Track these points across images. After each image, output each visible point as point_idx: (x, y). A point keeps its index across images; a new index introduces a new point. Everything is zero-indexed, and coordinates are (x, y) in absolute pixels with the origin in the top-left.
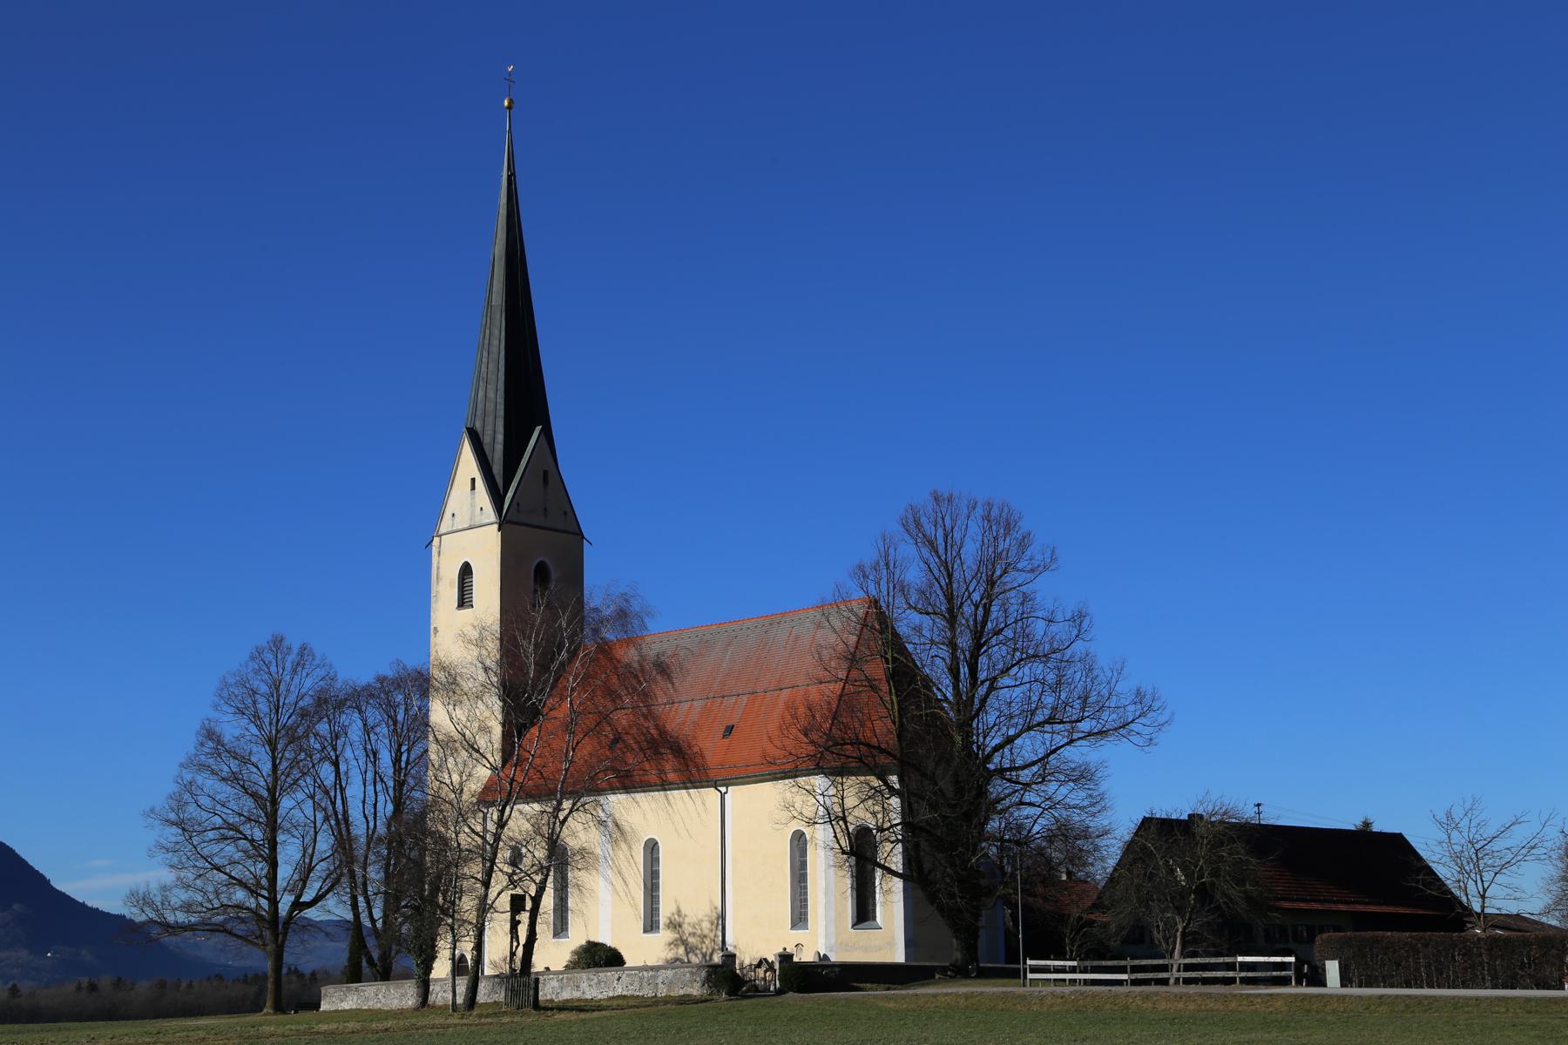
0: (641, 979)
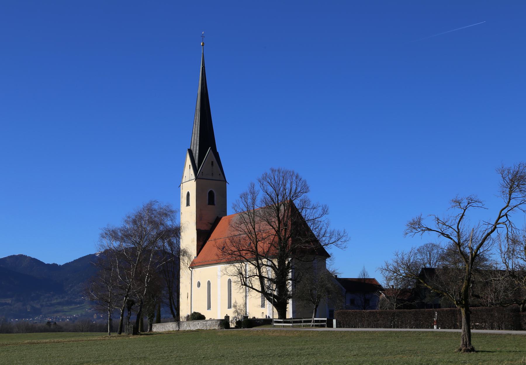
0: (203, 324)
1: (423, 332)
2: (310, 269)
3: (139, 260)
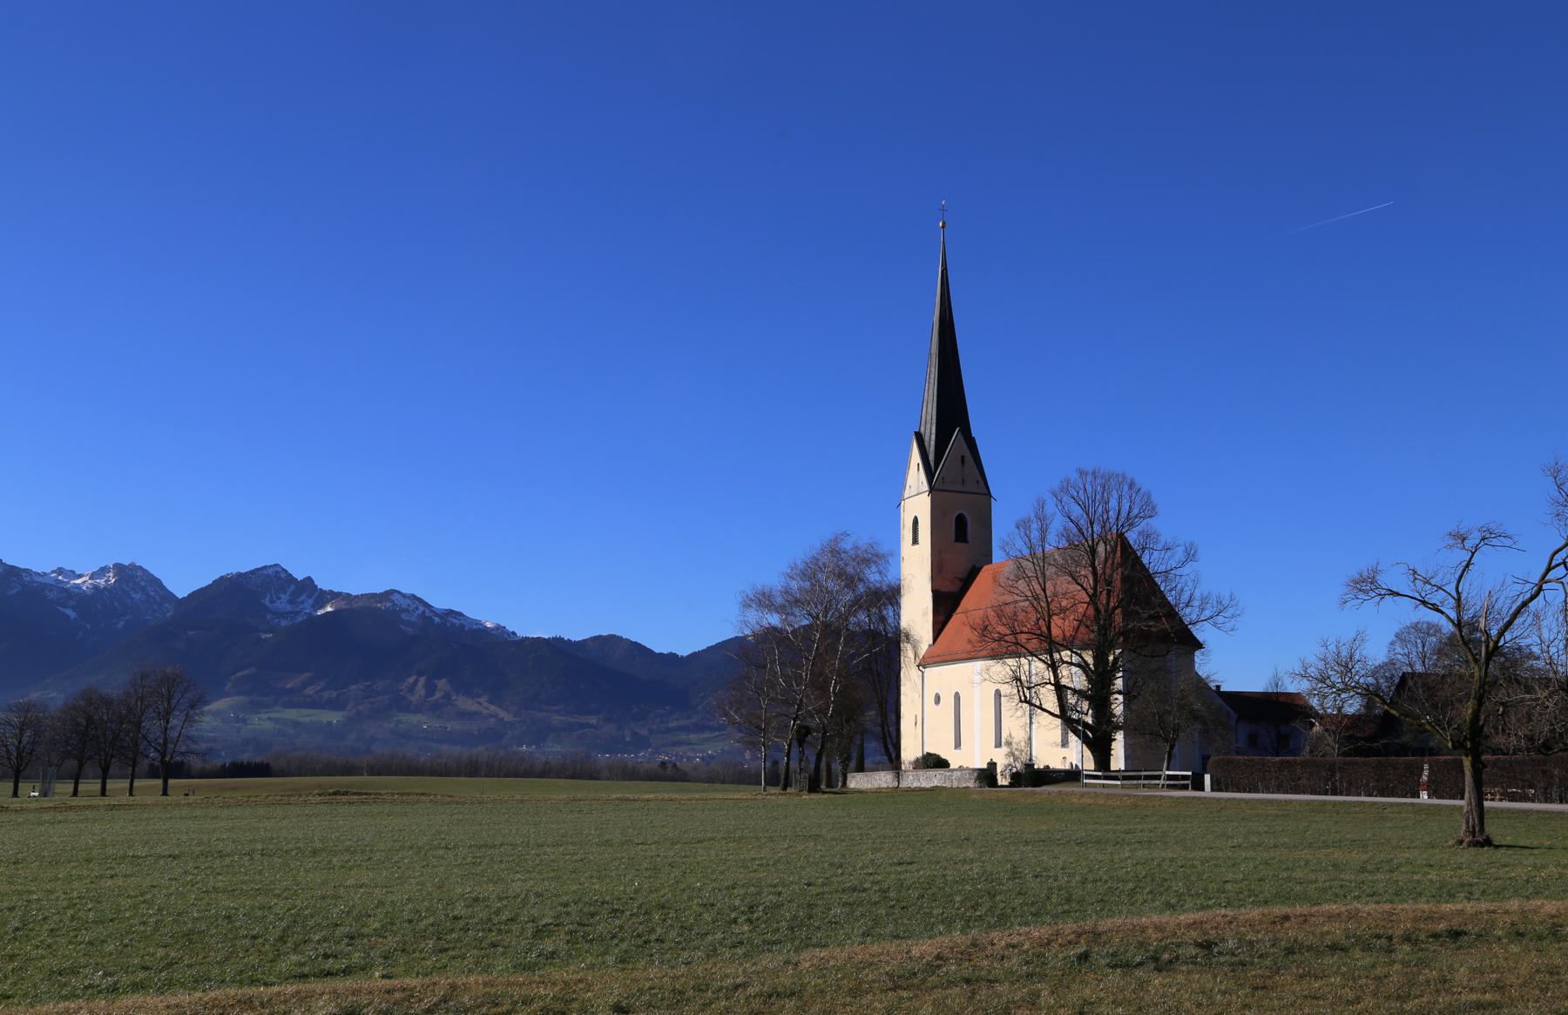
1: (1392, 805)
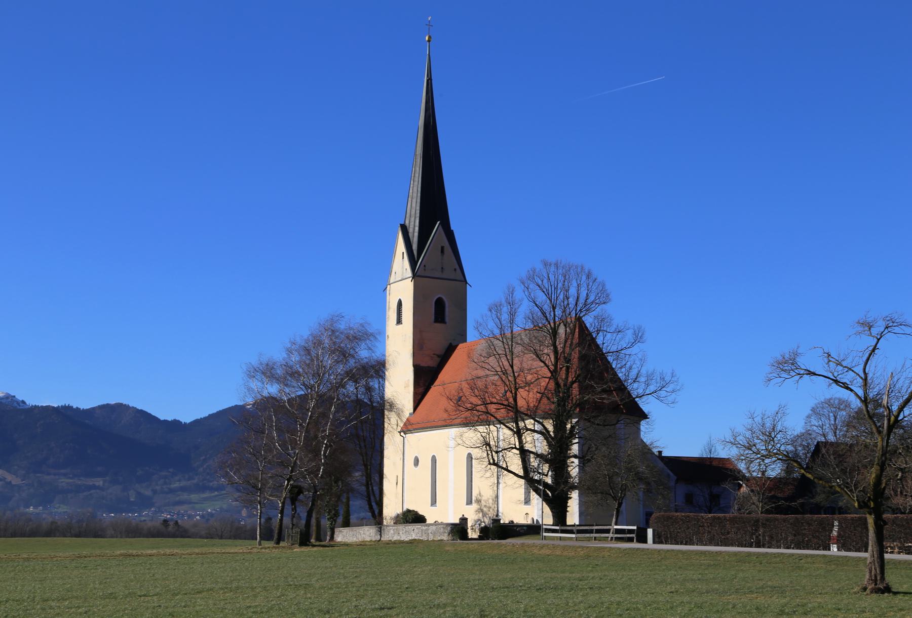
1: (807, 556)
2: (610, 439)
3: (311, 417)
